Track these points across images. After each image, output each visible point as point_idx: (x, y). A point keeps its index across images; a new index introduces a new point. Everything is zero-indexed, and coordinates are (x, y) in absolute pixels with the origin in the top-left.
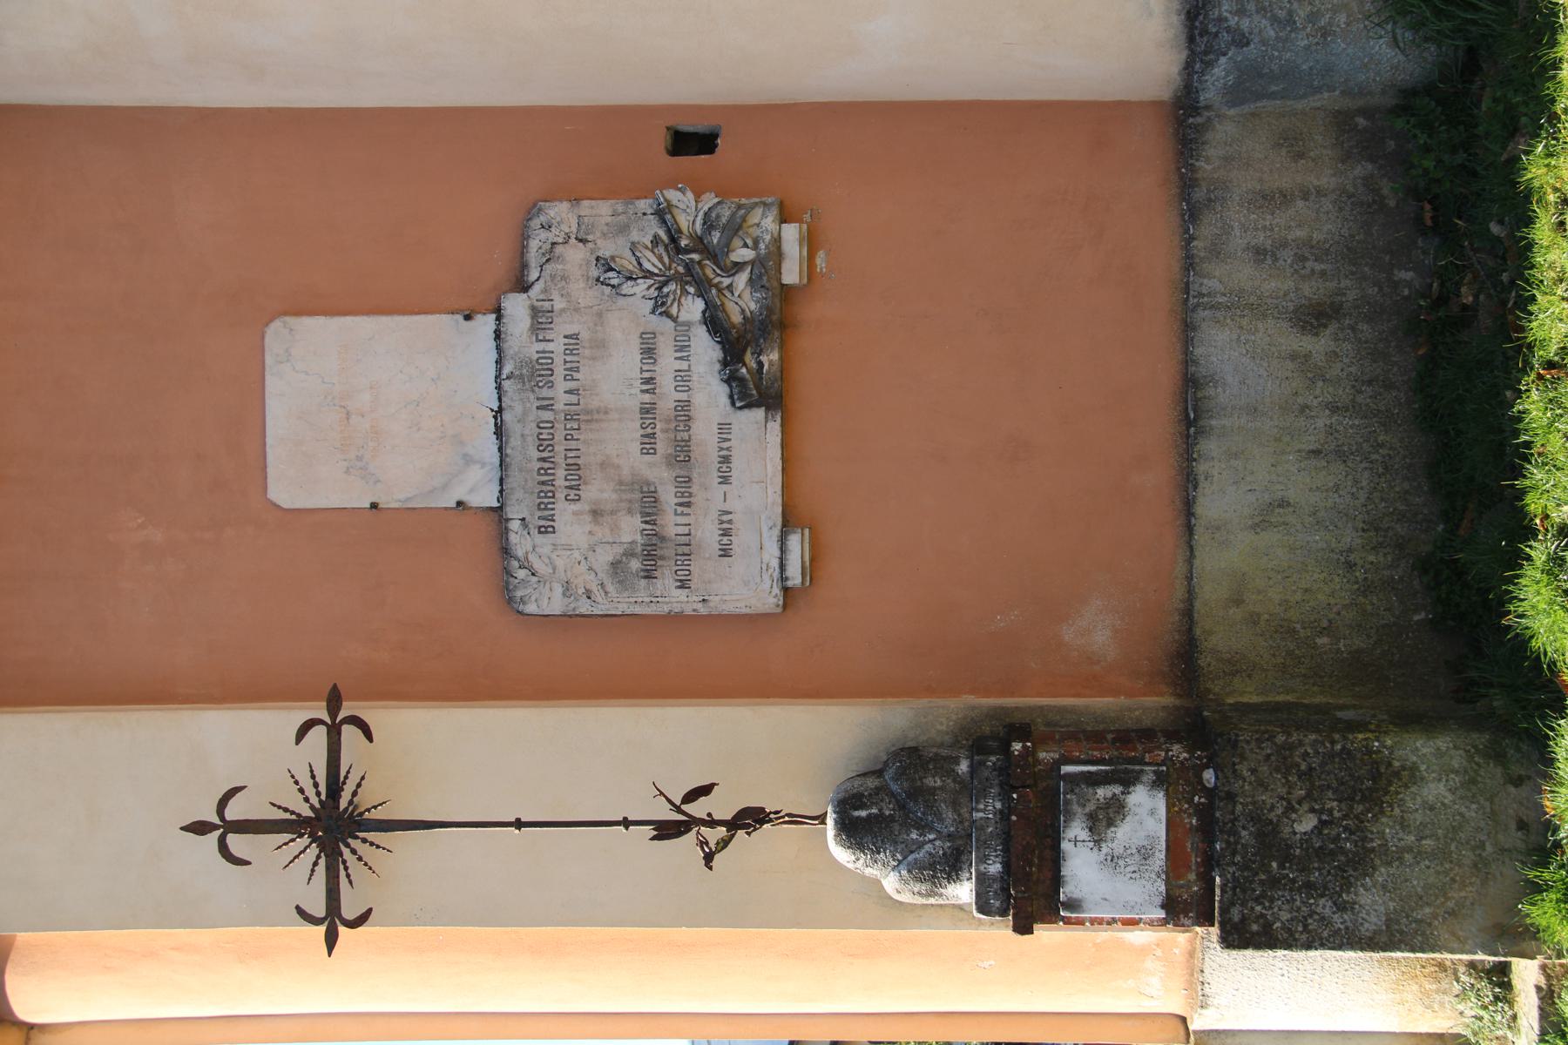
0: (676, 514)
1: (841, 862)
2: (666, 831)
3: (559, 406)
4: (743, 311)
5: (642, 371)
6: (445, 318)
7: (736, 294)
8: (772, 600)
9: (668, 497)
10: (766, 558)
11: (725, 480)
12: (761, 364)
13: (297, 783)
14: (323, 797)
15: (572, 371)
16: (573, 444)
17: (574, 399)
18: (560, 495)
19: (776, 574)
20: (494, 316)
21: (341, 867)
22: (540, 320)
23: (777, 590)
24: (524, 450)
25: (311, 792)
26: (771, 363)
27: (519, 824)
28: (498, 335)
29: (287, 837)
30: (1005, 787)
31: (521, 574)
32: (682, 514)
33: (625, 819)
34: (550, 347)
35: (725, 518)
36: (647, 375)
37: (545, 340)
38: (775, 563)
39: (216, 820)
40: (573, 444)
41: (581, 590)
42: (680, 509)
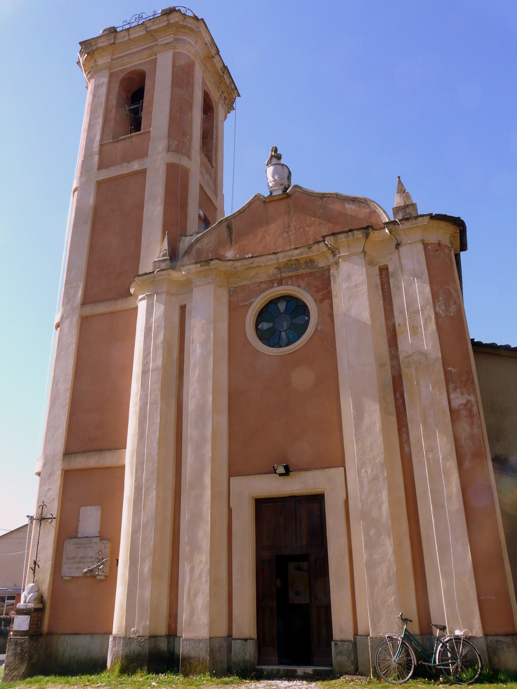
9: (75, 560)
15: (90, 547)
20: (99, 536)
22: (95, 543)
38: (66, 575)
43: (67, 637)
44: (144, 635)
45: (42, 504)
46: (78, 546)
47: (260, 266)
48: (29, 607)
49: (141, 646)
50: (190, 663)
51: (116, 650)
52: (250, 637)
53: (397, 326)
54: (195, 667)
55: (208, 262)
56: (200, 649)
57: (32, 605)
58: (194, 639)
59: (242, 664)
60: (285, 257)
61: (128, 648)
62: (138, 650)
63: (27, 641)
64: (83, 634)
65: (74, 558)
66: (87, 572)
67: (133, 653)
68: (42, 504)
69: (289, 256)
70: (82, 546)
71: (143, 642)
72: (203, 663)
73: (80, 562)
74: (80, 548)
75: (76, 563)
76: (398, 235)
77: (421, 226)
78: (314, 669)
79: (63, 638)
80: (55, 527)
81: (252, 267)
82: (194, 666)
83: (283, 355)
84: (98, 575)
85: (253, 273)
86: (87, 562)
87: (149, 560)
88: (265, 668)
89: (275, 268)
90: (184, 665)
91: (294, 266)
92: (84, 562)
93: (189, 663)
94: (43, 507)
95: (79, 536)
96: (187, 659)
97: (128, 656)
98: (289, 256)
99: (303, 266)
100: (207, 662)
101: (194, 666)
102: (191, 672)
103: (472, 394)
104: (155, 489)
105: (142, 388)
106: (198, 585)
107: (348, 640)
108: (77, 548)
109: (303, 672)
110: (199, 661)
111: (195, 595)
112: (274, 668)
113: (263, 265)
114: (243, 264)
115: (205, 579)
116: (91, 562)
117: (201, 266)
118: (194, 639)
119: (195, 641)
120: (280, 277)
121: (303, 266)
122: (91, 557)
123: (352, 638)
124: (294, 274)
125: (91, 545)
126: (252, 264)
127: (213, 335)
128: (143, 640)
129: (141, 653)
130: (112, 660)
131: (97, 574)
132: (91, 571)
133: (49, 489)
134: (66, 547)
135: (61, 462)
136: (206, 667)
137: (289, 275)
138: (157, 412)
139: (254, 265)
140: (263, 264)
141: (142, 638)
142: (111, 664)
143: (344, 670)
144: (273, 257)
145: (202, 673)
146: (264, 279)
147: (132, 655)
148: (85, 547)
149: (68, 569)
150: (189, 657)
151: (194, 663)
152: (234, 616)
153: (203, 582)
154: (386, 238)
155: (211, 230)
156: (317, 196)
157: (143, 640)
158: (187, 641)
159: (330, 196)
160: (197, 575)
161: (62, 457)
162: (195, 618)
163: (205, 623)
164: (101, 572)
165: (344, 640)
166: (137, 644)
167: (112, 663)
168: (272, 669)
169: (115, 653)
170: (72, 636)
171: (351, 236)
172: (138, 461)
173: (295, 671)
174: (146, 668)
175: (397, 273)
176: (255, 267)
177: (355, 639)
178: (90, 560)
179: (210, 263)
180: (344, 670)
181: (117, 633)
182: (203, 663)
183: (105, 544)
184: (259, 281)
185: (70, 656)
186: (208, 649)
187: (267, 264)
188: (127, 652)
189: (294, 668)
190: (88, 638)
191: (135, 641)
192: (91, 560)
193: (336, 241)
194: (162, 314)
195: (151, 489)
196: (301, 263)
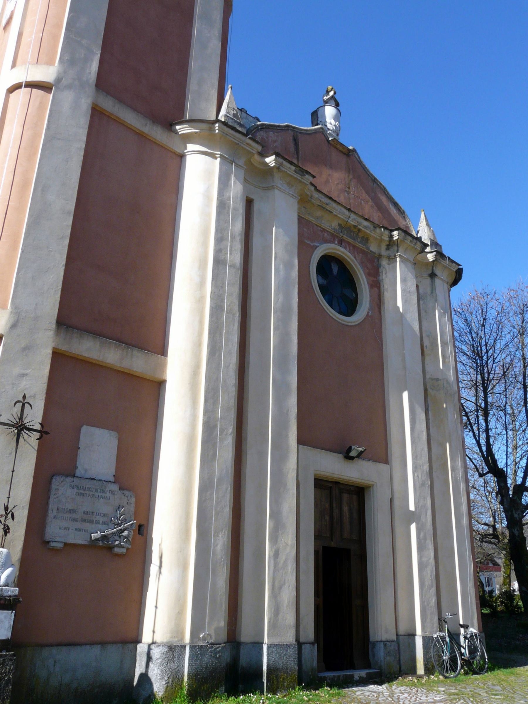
0: (70, 517)
1: (514, 572)
2: (6, 508)
3: (96, 493)
4: (110, 538)
5: (101, 513)
6: (114, 471)
7: (114, 537)
8: (47, 538)
9: (74, 516)
10: (57, 538)
11: (76, 530)
12: (100, 541)
13: (32, 421)
14: (27, 427)
15: (102, 497)
16: (88, 495)
17: (97, 497)
18: (77, 491)
19: (53, 540)
20: (114, 481)
21: (10, 427)
22: (113, 492)
23: (49, 540)
24: (89, 484)
25: (29, 424)
26: (100, 543)
27: (13, 471)
28: (110, 482)
29: (19, 416)
30: (470, 643)
31: (62, 479)
32: (70, 519)
33: (10, 497)
34: (108, 493)
35: (68, 529)
36: (100, 514)
37: (109, 492)
38: (56, 540)
39: (25, 401)
40: (88, 495)
41: (56, 492)
42: (71, 518)
43: (54, 650)
44: (217, 642)
45: (21, 399)
46: (82, 492)
47: (332, 212)
48: (9, 593)
49: (217, 658)
50: (277, 677)
51: (176, 667)
52: (381, 639)
53: (425, 348)
54: (283, 681)
55: (303, 172)
56: (288, 658)
57: (15, 590)
58: (282, 645)
59: (310, 674)
60: (355, 220)
61: (198, 662)
62: (212, 663)
63: (11, 660)
64: (86, 644)
65: (71, 511)
66: (97, 540)
67: (206, 668)
68: (21, 399)
69: (358, 222)
70: (87, 492)
71: (219, 652)
72: (292, 674)
73: (83, 521)
74: (83, 495)
75: (76, 520)
76: (436, 266)
77: (452, 270)
78: (367, 672)
79: (46, 652)
80: (36, 448)
81: (324, 208)
82: (281, 679)
83: (343, 324)
84: (119, 546)
85: (319, 213)
86: (98, 522)
87: (223, 533)
88: (327, 676)
89: (339, 223)
90: (271, 680)
91: (352, 233)
92: (91, 522)
93: (276, 676)
94: (23, 406)
95: (78, 473)
96: (274, 671)
97: (199, 675)
98: (358, 222)
99: (359, 240)
100: (296, 673)
101: (281, 679)
102: (279, 688)
103: (471, 432)
104: (231, 434)
105: (214, 282)
106: (284, 575)
107: (392, 640)
108: (78, 494)
109: (358, 676)
110: (286, 673)
111: (280, 588)
112: (335, 674)
113: (334, 213)
114: (320, 199)
115: (291, 567)
116: (104, 523)
117: (295, 171)
118: (282, 645)
119: (282, 647)
120: (341, 237)
121: (359, 240)
122: (105, 515)
123: (394, 638)
124: (352, 242)
125: (104, 495)
126: (327, 204)
127: (297, 263)
128: (220, 649)
129: (217, 668)
130: (168, 683)
131: (117, 545)
132: (104, 538)
133: (23, 375)
134: (57, 489)
135: (51, 333)
136: (295, 679)
137: (349, 241)
138: (234, 325)
139: (328, 208)
140: (335, 212)
141: (218, 646)
142: (166, 689)
143: (392, 670)
144: (346, 212)
145: (291, 687)
146: (328, 229)
147: (205, 671)
148: (93, 495)
149: (60, 528)
150: (275, 668)
151: (282, 675)
152: (301, 616)
153: (289, 571)
154: (424, 261)
155: (279, 128)
156: (370, 176)
157: (220, 649)
158: (273, 647)
159: (379, 184)
160: (282, 562)
161: (54, 326)
162: (280, 616)
163: (292, 624)
164: (123, 542)
165: (389, 640)
166: (211, 655)
167: (167, 687)
168: (334, 676)
169: (174, 671)
170: (64, 649)
171: (414, 243)
172: (208, 385)
173: (352, 676)
174: (223, 689)
175: (425, 298)
176: (327, 210)
177: (397, 638)
178: (102, 519)
179: (305, 175)
180: (392, 670)
181: (171, 640)
182: (292, 674)
183: (129, 497)
184: (323, 227)
185: (61, 685)
186: (297, 656)
187: (338, 215)
188: (196, 668)
189: (352, 673)
190: (96, 650)
191: (208, 650)
192: (105, 519)
193: (404, 239)
194: (239, 196)
195: (225, 433)
196: (359, 236)
